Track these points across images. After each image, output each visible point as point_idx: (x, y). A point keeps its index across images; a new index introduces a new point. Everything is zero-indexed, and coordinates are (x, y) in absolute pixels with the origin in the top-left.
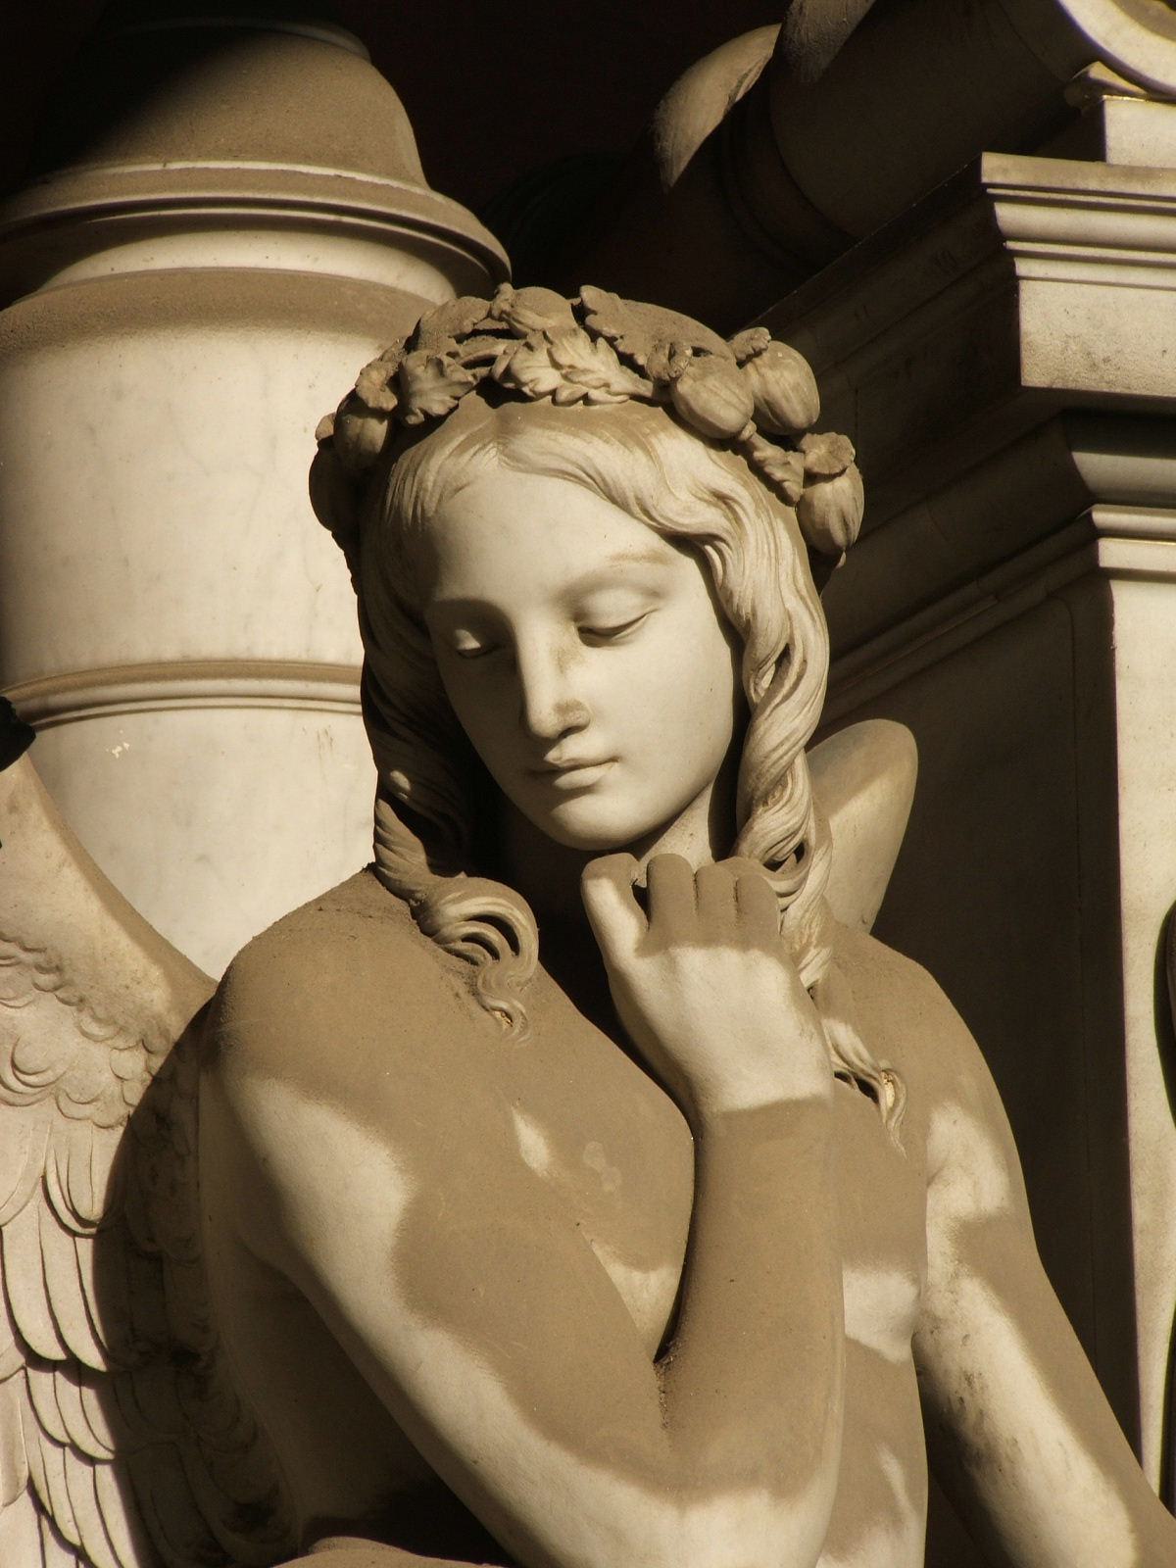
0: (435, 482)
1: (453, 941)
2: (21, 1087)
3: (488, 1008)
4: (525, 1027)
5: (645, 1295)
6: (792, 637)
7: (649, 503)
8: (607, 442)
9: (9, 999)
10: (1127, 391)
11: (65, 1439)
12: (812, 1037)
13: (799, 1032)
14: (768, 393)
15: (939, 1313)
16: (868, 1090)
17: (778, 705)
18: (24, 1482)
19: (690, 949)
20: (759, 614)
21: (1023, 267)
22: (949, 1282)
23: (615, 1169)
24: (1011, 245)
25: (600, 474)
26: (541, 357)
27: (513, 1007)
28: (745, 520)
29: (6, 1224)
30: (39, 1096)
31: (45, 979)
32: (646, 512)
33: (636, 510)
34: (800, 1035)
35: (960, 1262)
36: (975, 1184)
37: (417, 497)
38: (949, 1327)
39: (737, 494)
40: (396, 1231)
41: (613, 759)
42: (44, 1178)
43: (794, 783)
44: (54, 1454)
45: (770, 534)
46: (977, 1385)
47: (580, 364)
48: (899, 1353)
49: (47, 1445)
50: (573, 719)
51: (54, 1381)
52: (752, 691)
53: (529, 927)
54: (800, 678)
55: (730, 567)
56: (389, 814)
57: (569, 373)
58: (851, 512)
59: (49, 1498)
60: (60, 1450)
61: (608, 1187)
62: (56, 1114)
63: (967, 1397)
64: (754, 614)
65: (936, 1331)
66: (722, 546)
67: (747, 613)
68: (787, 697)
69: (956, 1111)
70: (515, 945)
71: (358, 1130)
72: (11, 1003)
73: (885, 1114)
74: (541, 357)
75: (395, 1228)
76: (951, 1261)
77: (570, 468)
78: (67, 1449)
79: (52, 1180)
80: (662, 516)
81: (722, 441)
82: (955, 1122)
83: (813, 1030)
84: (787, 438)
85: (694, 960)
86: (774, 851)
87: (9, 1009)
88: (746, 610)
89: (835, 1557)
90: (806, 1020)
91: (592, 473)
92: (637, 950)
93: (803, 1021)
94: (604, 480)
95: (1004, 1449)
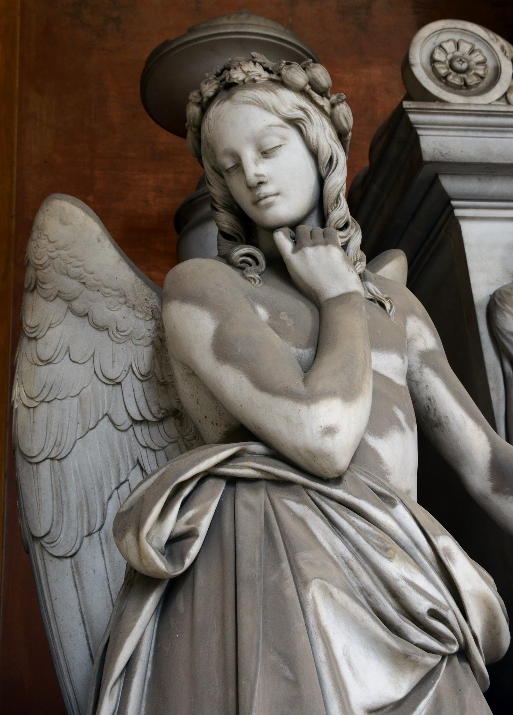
0: (212, 117)
1: (238, 264)
2: (123, 338)
3: (247, 277)
4: (260, 282)
5: (304, 357)
6: (332, 153)
7: (277, 108)
8: (261, 91)
9: (112, 308)
10: (452, 161)
11: (146, 446)
12: (352, 272)
13: (347, 270)
14: (313, 76)
15: (418, 380)
16: (383, 306)
17: (330, 175)
18: (136, 461)
19: (308, 248)
20: (319, 144)
21: (419, 132)
22: (419, 370)
23: (291, 320)
24: (415, 126)
25: (260, 100)
26: (239, 70)
27: (255, 276)
28: (311, 115)
29: (122, 381)
30: (126, 339)
31: (122, 300)
32: (277, 112)
33: (273, 111)
34: (348, 271)
35: (422, 363)
36: (425, 341)
37: (208, 124)
38: (421, 384)
39: (307, 107)
40: (213, 337)
41: (277, 194)
42: (131, 365)
43: (341, 201)
44: (144, 451)
45: (320, 120)
46: (432, 401)
47: (250, 70)
48: (401, 381)
49: (141, 448)
50: (261, 179)
51: (141, 428)
52: (323, 172)
53: (261, 256)
54: (336, 165)
55: (308, 130)
56: (221, 238)
57: (247, 73)
58: (347, 116)
59: (144, 464)
60: (145, 449)
61: (289, 325)
62: (132, 344)
63: (430, 405)
64: (318, 144)
65: (417, 386)
66: (304, 122)
67: (316, 145)
68: (333, 172)
69: (415, 318)
70: (257, 263)
71: (199, 308)
72: (113, 310)
73: (388, 312)
74: (239, 70)
75: (212, 336)
76: (420, 363)
77: (251, 100)
78: (147, 449)
79: (133, 365)
80: (282, 112)
81: (302, 92)
82: (415, 321)
83: (353, 270)
84: (323, 93)
85: (310, 251)
86: (337, 224)
87: (113, 312)
88: (315, 143)
89: (379, 437)
90: (350, 267)
91: (257, 100)
92: (292, 252)
93: (348, 267)
94: (261, 102)
95: (443, 420)
